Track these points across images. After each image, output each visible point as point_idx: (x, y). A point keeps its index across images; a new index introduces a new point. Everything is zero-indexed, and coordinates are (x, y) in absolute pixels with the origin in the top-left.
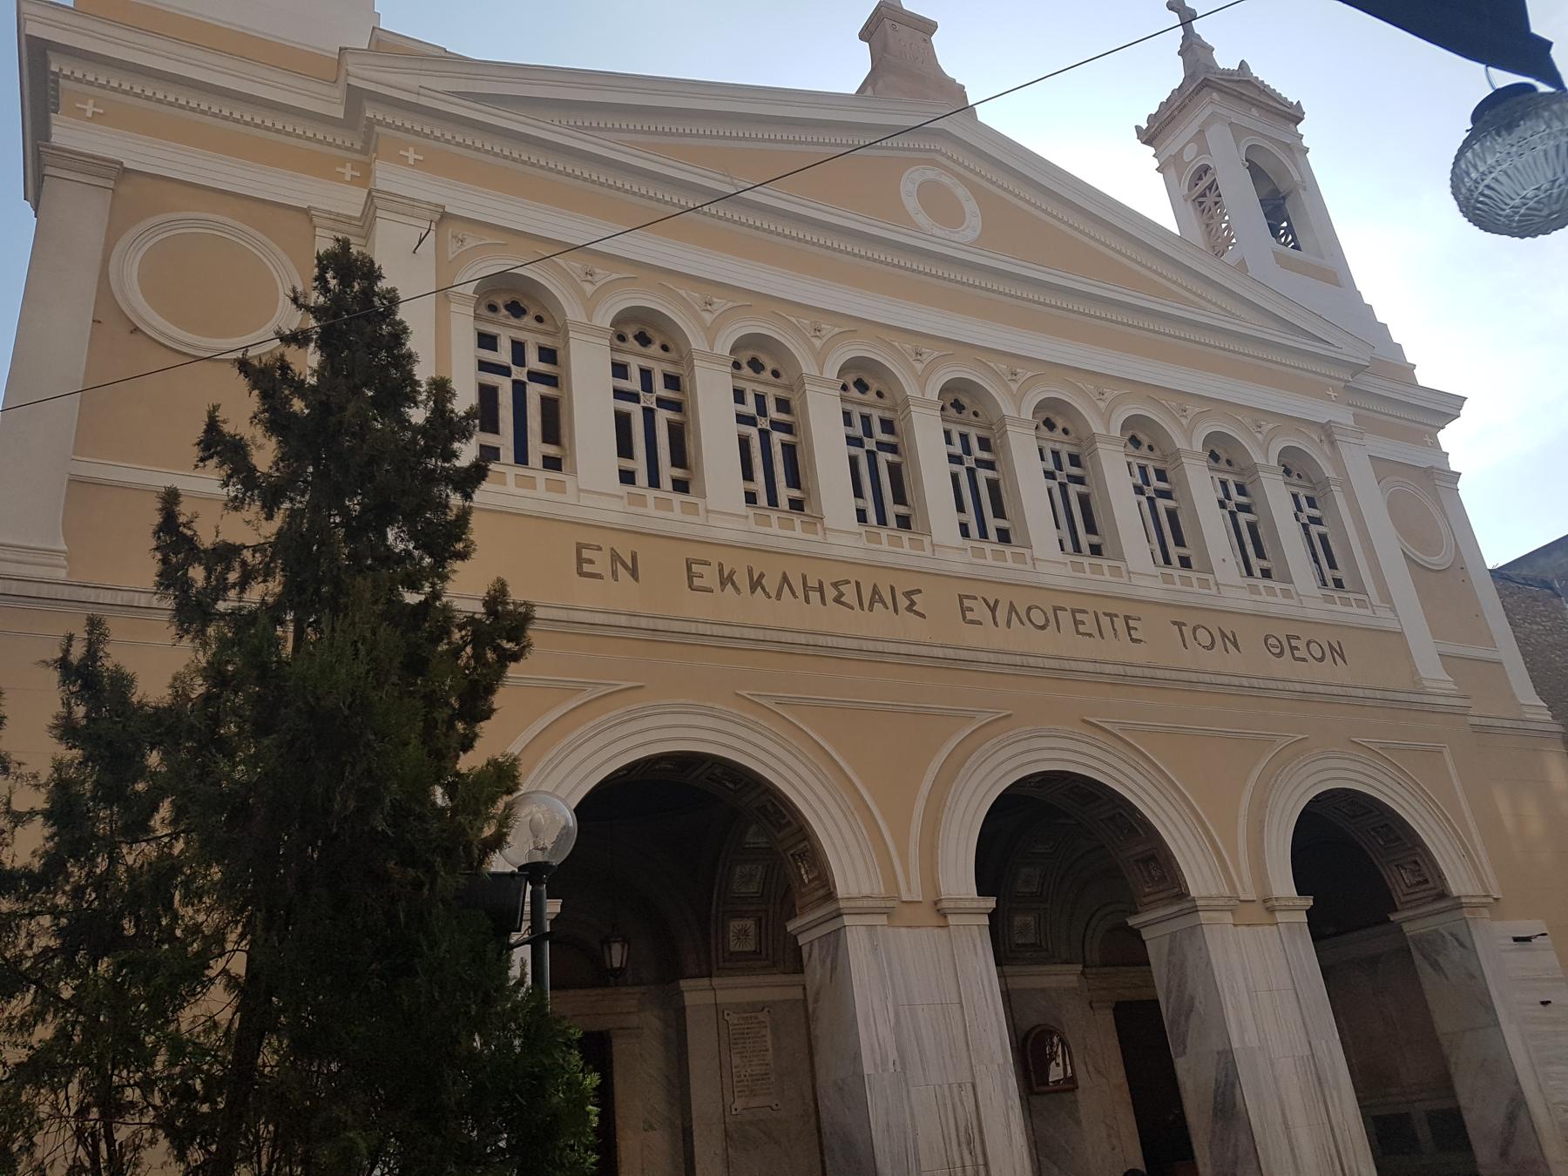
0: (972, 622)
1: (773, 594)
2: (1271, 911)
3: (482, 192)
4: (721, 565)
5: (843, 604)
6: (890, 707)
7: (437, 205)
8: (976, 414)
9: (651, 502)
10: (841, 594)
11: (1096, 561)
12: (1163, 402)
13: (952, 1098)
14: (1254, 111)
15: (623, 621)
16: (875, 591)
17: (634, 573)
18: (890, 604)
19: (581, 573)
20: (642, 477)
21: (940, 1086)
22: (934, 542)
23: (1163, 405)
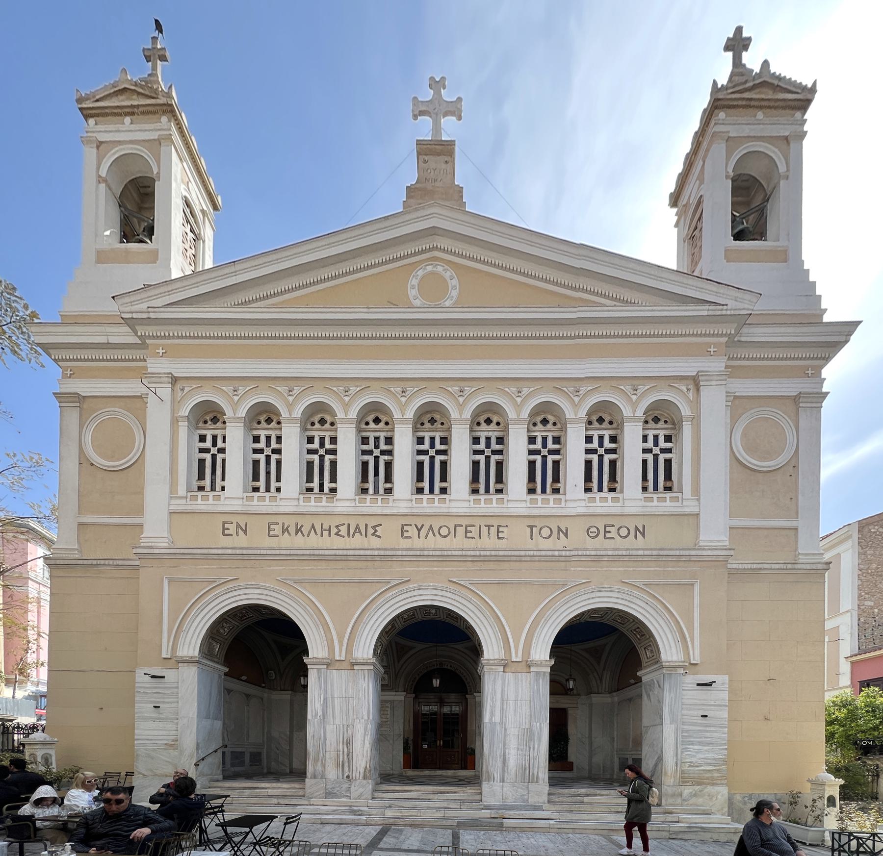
0: (406, 537)
2: (529, 666)
3: (202, 361)
4: (283, 523)
5: (339, 535)
7: (168, 373)
8: (442, 424)
10: (376, 531)
11: (556, 496)
12: (565, 389)
14: (760, 115)
15: (230, 551)
16: (357, 527)
17: (245, 532)
18: (364, 533)
19: (224, 535)
20: (427, 489)
23: (507, 392)
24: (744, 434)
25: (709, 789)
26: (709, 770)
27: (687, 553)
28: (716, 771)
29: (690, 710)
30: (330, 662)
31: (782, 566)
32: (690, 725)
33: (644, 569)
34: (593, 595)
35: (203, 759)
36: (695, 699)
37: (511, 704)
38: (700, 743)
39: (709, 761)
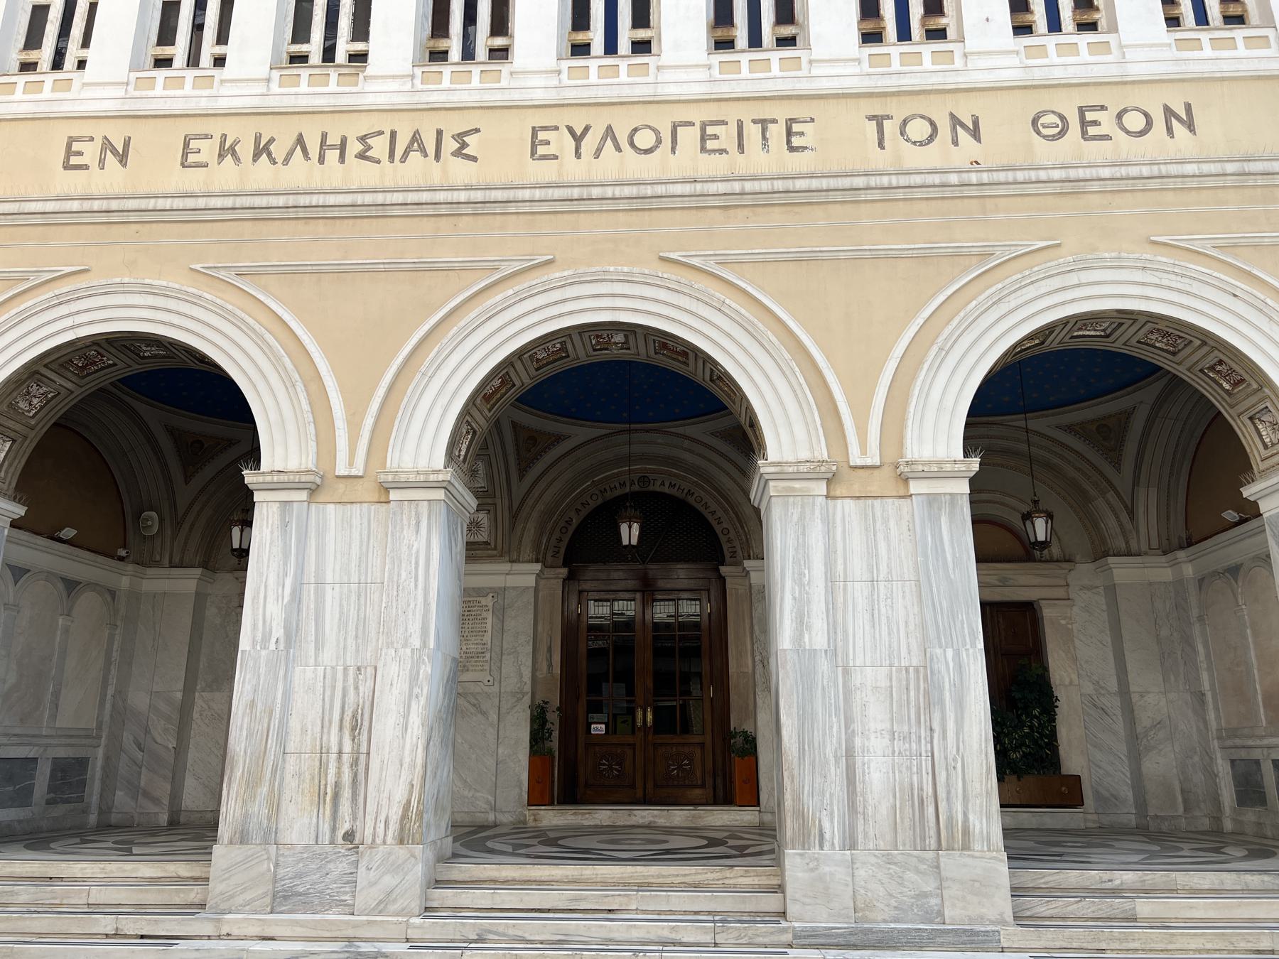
1: (280, 159)
6: (310, 268)
9: (1051, 49)
13: (345, 680)
21: (333, 668)
22: (1123, 43)
34: (1073, 279)
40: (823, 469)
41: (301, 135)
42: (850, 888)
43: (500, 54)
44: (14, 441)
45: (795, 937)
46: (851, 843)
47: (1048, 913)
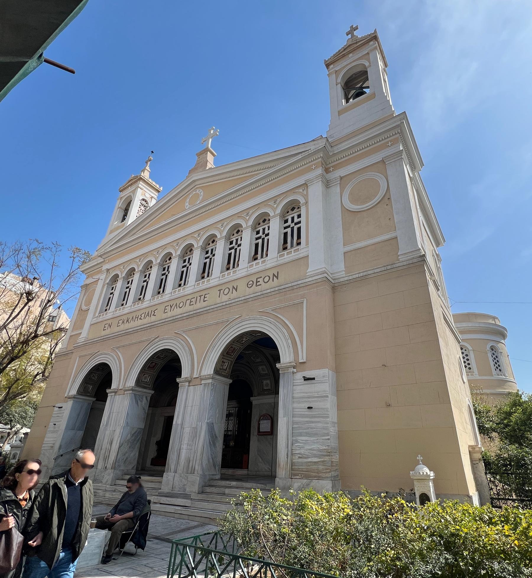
23: (269, 205)
24: (351, 194)
25: (315, 482)
26: (315, 462)
27: (296, 283)
28: (321, 463)
29: (299, 402)
30: (295, 365)
31: (383, 269)
32: (300, 417)
33: (273, 300)
34: (241, 325)
35: (62, 455)
36: (303, 393)
37: (189, 408)
38: (308, 434)
39: (315, 452)
40: (186, 380)
41: (273, 274)
42: (172, 483)
43: (299, 244)
44: (93, 386)
45: (158, 494)
46: (175, 472)
47: (209, 491)
